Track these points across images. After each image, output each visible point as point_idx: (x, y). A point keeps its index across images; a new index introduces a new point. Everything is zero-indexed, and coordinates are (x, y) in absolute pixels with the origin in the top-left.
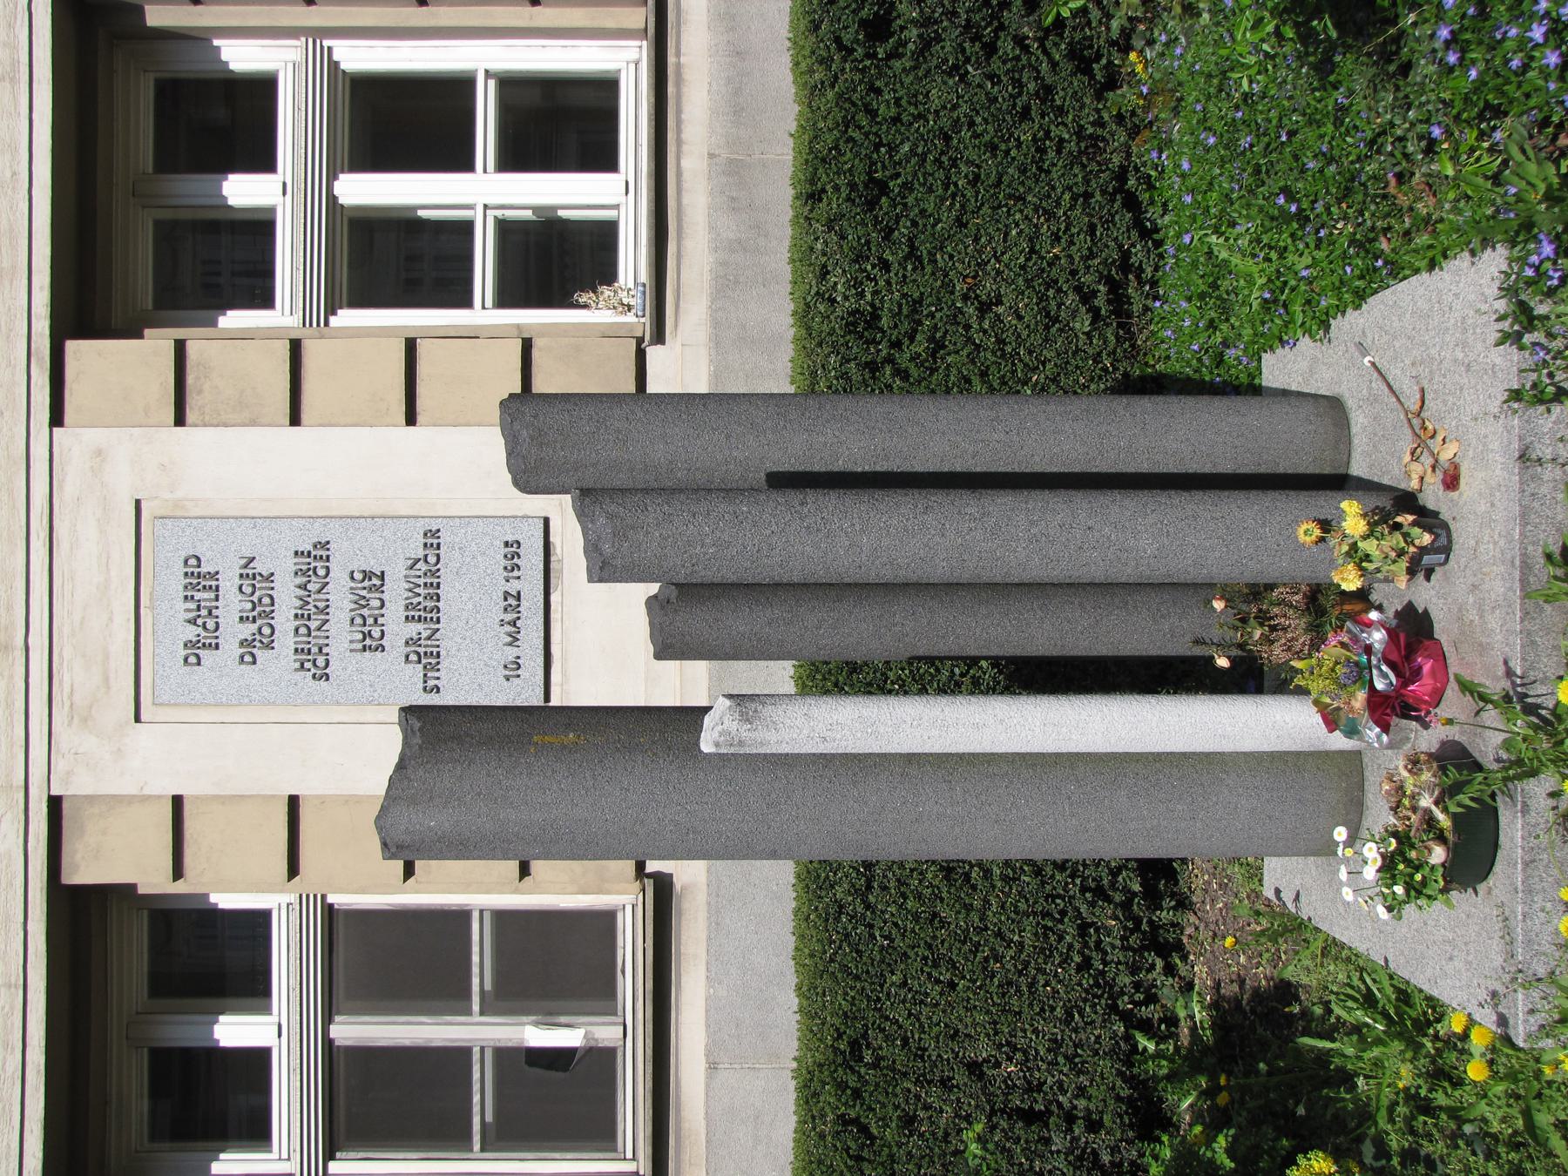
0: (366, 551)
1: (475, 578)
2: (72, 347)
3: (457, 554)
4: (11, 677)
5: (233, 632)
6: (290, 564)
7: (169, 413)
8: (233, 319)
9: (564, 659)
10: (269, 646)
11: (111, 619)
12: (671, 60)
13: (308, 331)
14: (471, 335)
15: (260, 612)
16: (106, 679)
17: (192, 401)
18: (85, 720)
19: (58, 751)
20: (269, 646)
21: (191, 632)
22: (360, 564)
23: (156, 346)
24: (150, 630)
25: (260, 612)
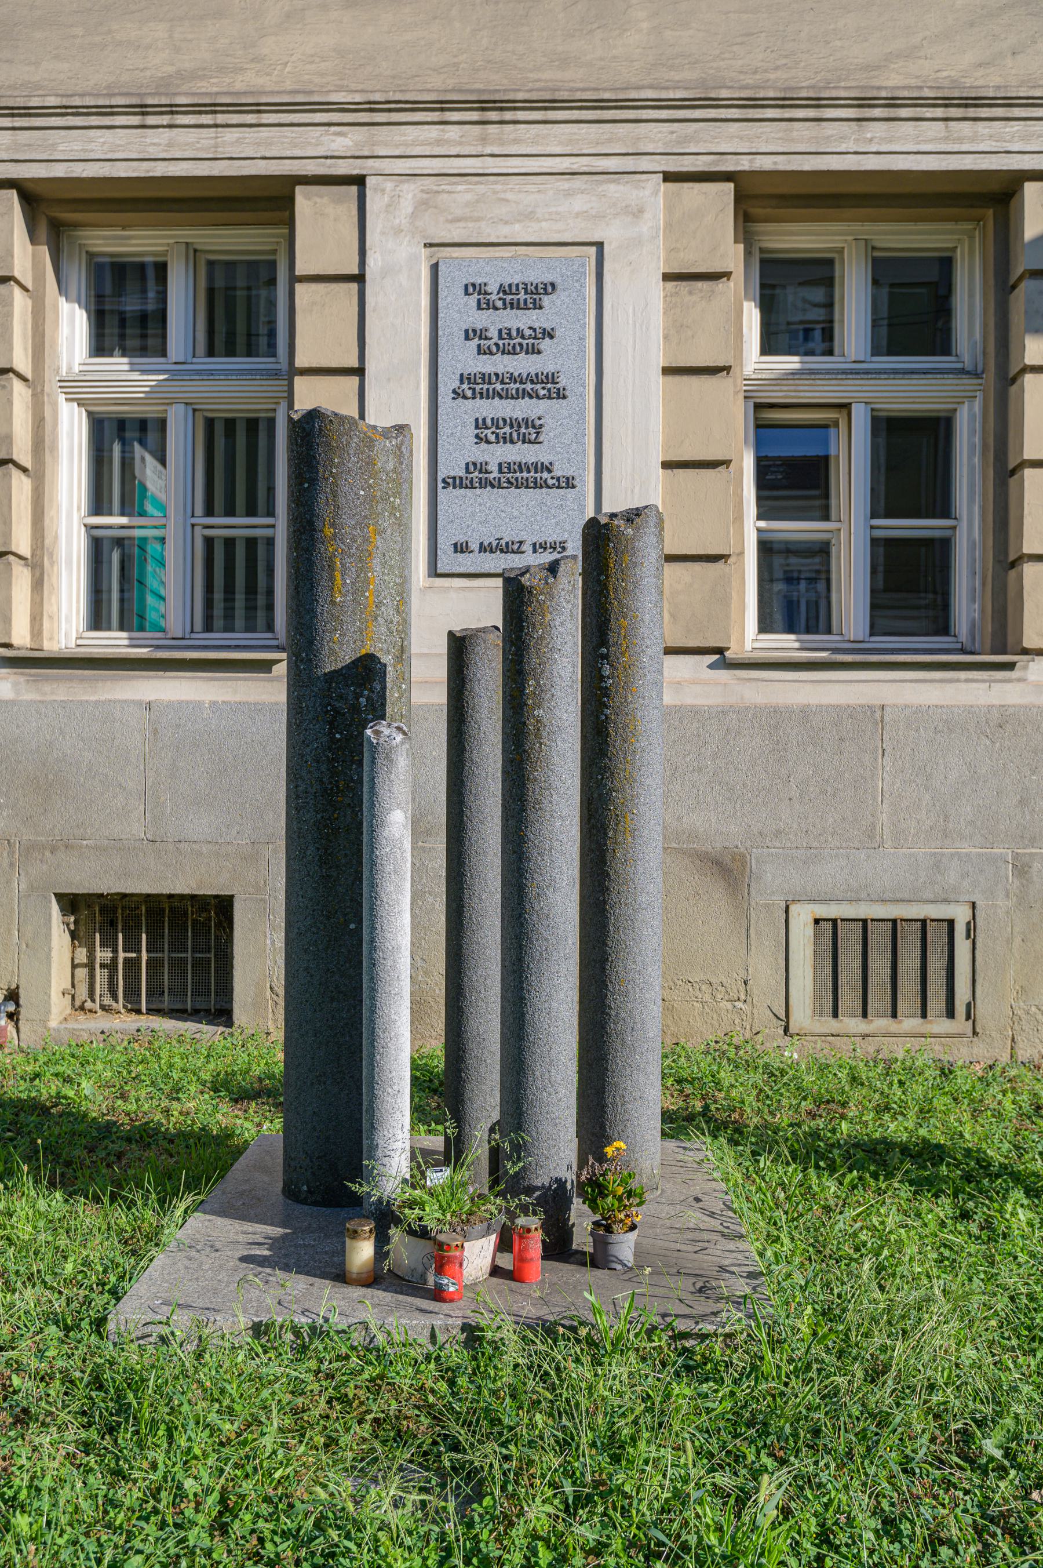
0: (560, 430)
1: (538, 518)
2: (728, 188)
3: (558, 503)
4: (461, 144)
5: (494, 321)
6: (550, 368)
7: (720, 565)
8: (752, 317)
9: (471, 589)
10: (480, 351)
11: (506, 223)
12: (963, 675)
13: (740, 382)
14: (739, 518)
15: (512, 343)
16: (458, 220)
17: (684, 286)
18: (423, 205)
19: (401, 182)
20: (480, 351)
21: (493, 288)
22: (547, 421)
23: (731, 256)
24: (497, 255)
25: (512, 343)
